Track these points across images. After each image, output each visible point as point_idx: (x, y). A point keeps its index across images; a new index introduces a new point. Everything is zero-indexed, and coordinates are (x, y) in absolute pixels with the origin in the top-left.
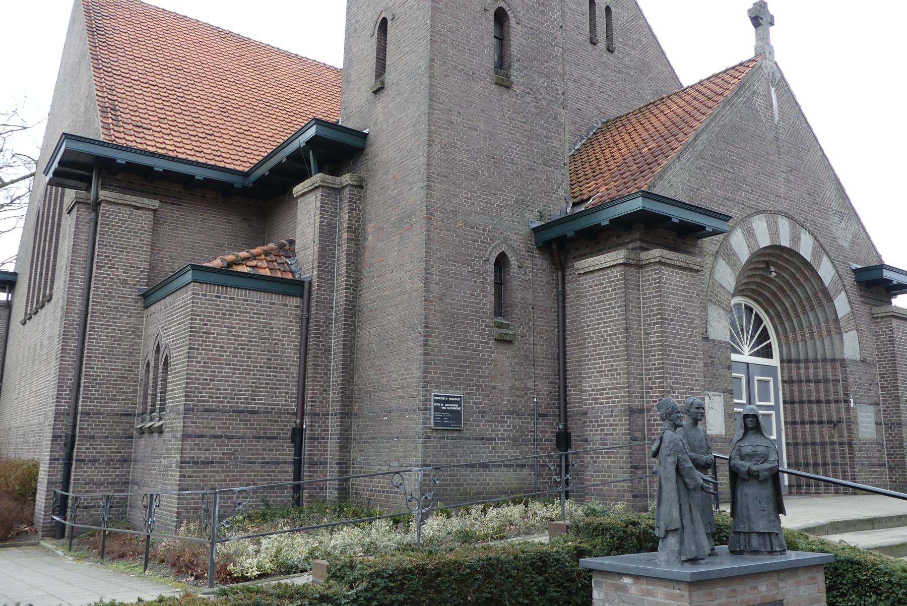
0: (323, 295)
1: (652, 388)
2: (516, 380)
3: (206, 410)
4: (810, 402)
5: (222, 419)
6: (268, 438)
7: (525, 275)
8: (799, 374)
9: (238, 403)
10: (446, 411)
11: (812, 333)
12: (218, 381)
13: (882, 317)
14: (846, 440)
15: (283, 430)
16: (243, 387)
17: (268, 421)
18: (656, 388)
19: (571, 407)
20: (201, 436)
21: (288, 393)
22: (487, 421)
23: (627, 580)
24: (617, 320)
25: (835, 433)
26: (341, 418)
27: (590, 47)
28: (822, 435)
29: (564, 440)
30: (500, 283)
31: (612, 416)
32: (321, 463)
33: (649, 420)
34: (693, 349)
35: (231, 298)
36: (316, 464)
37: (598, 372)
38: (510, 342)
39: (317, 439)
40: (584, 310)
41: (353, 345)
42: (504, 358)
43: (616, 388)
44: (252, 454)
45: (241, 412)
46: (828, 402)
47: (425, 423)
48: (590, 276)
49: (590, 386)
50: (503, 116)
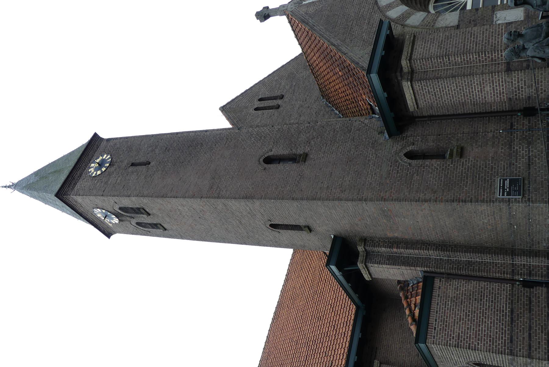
0: (432, 264)
2: (487, 144)
3: (511, 342)
6: (530, 303)
7: (418, 141)
9: (506, 321)
10: (510, 188)
12: (490, 332)
15: (524, 293)
17: (518, 302)
19: (506, 108)
20: (530, 346)
21: (498, 289)
22: (516, 162)
27: (281, 109)
31: (512, 82)
34: (465, 34)
38: (462, 149)
39: (530, 271)
40: (440, 104)
45: (512, 319)
47: (519, 202)
50: (323, 157)
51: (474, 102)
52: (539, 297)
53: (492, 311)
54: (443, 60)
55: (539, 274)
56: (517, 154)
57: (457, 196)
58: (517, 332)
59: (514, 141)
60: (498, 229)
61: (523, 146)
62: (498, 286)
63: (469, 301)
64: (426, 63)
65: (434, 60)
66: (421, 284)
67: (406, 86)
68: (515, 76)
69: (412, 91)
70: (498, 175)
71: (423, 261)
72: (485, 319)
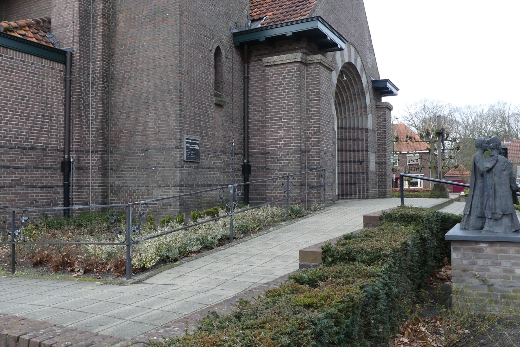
0: (83, 64)
1: (311, 138)
4: (350, 151)
5: (9, 154)
6: (44, 168)
7: (229, 63)
8: (346, 135)
9: (21, 141)
11: (353, 114)
12: (5, 123)
13: (381, 108)
14: (365, 171)
15: (55, 162)
16: (24, 129)
17: (44, 156)
18: (314, 138)
19: (251, 149)
21: (57, 135)
22: (211, 157)
23: (482, 245)
24: (293, 97)
25: (360, 167)
26: (102, 154)
28: (355, 168)
29: (247, 170)
30: (217, 67)
31: (288, 154)
32: (86, 186)
33: (308, 157)
35: (11, 58)
36: (82, 186)
37: (278, 128)
39: (83, 169)
40: (268, 89)
41: (108, 103)
42: (218, 115)
43: (292, 138)
44: (34, 180)
45: (24, 148)
46: (358, 151)
47: (181, 157)
48: (273, 68)
49: (273, 136)
51: (268, 121)
52: (52, 177)
53: (32, 126)
54: (314, 95)
55: (80, 177)
56: (217, 157)
57: (184, 96)
58: (10, 154)
59: (226, 156)
60: (138, 137)
61: (222, 163)
62: (60, 136)
63: (41, 101)
64: (314, 79)
65: (317, 86)
66: (52, 46)
67: (298, 56)
68: (294, 157)
69: (288, 61)
70: (202, 139)
71: (86, 53)
72: (21, 119)
